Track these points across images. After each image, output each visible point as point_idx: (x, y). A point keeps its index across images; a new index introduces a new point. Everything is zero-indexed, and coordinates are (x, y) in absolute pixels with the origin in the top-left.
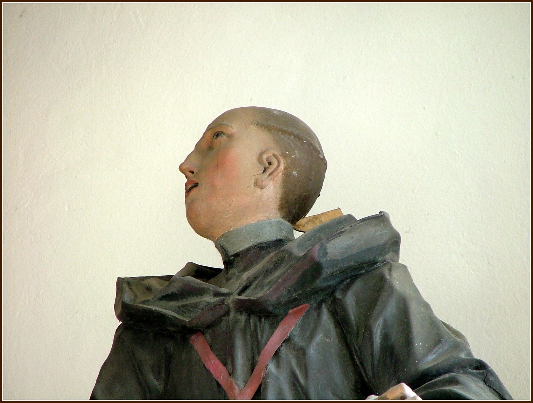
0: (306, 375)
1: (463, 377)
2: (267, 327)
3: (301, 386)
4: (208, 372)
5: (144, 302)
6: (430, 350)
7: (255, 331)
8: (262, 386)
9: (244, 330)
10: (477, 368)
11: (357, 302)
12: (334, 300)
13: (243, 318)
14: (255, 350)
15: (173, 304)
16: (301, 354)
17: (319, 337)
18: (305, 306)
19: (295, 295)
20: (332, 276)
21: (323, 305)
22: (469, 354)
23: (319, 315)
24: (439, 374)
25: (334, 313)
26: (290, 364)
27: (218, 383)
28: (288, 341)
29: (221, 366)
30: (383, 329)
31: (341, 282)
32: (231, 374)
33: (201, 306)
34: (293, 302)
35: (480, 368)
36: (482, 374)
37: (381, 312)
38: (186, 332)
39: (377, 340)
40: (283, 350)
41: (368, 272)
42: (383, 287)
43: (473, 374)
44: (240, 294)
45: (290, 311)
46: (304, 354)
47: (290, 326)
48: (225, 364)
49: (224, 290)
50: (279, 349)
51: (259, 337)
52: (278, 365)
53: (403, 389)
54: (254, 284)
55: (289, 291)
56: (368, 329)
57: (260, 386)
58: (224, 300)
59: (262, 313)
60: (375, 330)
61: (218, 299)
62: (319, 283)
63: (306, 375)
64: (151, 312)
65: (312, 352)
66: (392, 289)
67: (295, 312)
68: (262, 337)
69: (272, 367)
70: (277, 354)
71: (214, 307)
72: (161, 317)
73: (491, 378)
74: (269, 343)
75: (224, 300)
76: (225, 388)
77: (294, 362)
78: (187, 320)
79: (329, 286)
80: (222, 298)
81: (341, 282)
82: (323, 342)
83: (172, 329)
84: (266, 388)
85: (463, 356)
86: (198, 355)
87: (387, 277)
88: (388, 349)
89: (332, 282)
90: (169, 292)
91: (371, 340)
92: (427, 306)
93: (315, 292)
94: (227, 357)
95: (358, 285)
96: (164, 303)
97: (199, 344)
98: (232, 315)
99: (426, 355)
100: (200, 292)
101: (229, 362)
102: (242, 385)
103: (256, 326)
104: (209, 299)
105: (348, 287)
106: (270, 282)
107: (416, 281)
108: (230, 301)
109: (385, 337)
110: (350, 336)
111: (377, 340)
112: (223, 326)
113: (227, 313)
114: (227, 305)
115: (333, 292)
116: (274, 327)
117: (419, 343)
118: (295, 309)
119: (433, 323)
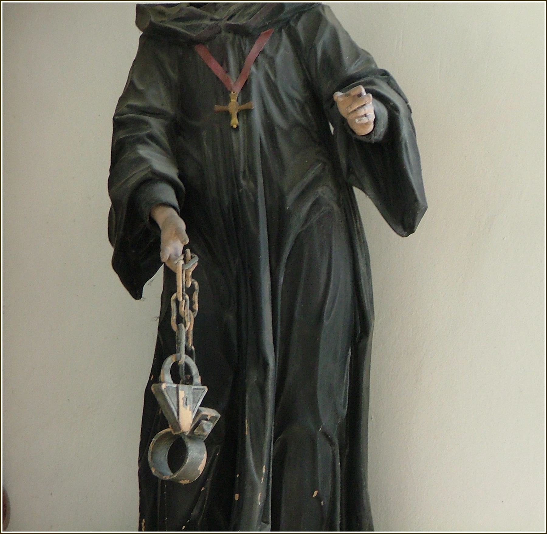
0: (275, 76)
1: (377, 81)
2: (247, 42)
3: (272, 81)
4: (210, 69)
5: (161, 22)
6: (353, 62)
7: (240, 44)
8: (248, 81)
9: (233, 44)
10: (383, 75)
11: (304, 29)
12: (290, 27)
13: (230, 36)
14: (242, 57)
15: (182, 24)
16: (271, 61)
17: (282, 51)
18: (272, 30)
19: (267, 23)
20: (289, 12)
21: (283, 30)
22: (376, 66)
23: (281, 36)
24: (360, 78)
25: (289, 35)
26: (264, 67)
27: (217, 78)
28: (262, 52)
29: (219, 67)
30: (322, 48)
31: (293, 16)
32: (228, 72)
33: (203, 26)
34: (264, 27)
35: (385, 73)
36: (387, 78)
37: (322, 36)
38: (192, 43)
39: (319, 54)
40: (260, 59)
41: (309, 10)
42: (321, 20)
43: (380, 79)
44: (228, 20)
45: (262, 33)
46: (274, 61)
47: (262, 43)
48: (222, 65)
49: (216, 17)
50: (257, 57)
51: (244, 49)
52: (257, 68)
53: (361, 89)
54: (238, 14)
55: (263, 20)
56: (313, 47)
57: (247, 80)
58: (217, 24)
59: (244, 33)
60: (318, 48)
61: (213, 22)
62: (282, 16)
63: (275, 76)
64: (170, 29)
65: (278, 60)
66: (327, 22)
67: (265, 34)
68: (245, 48)
69: (253, 69)
70: (256, 61)
71: (211, 28)
72: (175, 33)
73: (392, 82)
74: (251, 53)
75: (217, 24)
76: (223, 81)
77: (267, 66)
78: (195, 35)
79: (287, 18)
80: (217, 22)
81: (293, 16)
82: (284, 54)
83: (182, 40)
84: (251, 83)
85: (373, 66)
86: (201, 58)
87: (323, 13)
88: (326, 59)
89: (289, 16)
90: (180, 16)
91: (316, 53)
92: (347, 33)
93: (279, 21)
94: (223, 61)
95: (303, 18)
96: (175, 23)
97: (201, 51)
98: (223, 34)
99: (351, 65)
100: (202, 17)
101: (225, 64)
102: (235, 79)
103: (240, 41)
104: (207, 22)
105: (298, 19)
106: (249, 14)
107: (338, 17)
108: (222, 24)
109: (324, 53)
110: (302, 52)
111: (319, 54)
112: (217, 41)
113: (220, 32)
114: (220, 27)
115: (288, 22)
116: (252, 43)
117: (346, 58)
118: (265, 32)
119: (352, 45)
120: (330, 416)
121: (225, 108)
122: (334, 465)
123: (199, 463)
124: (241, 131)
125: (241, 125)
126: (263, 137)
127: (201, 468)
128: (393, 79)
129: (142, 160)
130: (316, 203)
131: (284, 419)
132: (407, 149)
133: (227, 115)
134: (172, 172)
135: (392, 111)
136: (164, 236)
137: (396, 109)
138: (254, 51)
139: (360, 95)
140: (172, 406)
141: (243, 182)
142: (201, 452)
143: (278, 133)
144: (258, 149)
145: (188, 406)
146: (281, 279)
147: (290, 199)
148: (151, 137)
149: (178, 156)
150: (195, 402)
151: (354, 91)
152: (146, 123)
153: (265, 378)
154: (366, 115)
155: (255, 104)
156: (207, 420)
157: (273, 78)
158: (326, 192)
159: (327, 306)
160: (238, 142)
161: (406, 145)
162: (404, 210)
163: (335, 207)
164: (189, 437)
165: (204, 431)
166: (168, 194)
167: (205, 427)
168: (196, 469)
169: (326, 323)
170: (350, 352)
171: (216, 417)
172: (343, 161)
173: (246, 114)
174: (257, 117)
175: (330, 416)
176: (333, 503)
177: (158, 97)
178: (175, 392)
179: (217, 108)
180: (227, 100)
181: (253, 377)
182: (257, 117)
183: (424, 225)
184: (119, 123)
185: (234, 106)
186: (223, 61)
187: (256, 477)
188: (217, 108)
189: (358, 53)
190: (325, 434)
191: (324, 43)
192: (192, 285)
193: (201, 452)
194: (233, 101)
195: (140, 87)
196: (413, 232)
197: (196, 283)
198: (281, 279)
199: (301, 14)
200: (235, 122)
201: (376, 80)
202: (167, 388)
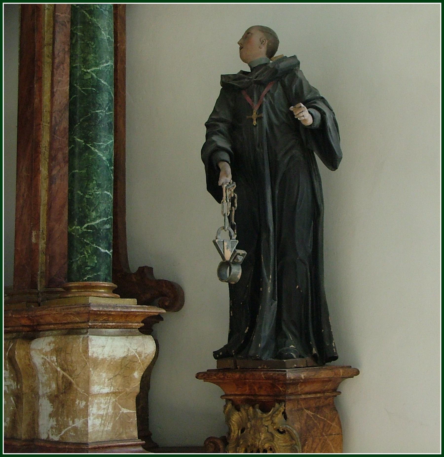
0: (274, 102)
6: (308, 94)
17: (277, 91)
22: (319, 95)
27: (249, 104)
32: (253, 101)
35: (322, 98)
38: (240, 90)
39: (294, 91)
40: (268, 95)
52: (266, 99)
69: (264, 99)
72: (233, 86)
77: (270, 98)
88: (296, 93)
92: (307, 82)
94: (252, 97)
97: (244, 93)
109: (296, 90)
111: (294, 91)
117: (305, 92)
119: (309, 86)
120: (303, 252)
121: (250, 117)
122: (307, 273)
123: (238, 275)
124: (257, 127)
125: (258, 124)
126: (268, 129)
127: (239, 277)
128: (326, 101)
129: (214, 141)
130: (292, 157)
131: (281, 253)
132: (330, 131)
133: (252, 120)
134: (227, 146)
135: (323, 114)
136: (221, 173)
137: (325, 113)
138: (265, 92)
139: (301, 107)
140: (221, 249)
141: (258, 149)
142: (239, 270)
143: (275, 127)
144: (265, 134)
145: (229, 250)
146: (277, 192)
147: (280, 156)
148: (220, 132)
149: (232, 139)
150: (232, 247)
151: (297, 106)
152: (218, 125)
153: (269, 236)
154: (303, 116)
155: (264, 115)
156: (240, 255)
157: (273, 103)
158: (297, 152)
159: (298, 203)
160: (256, 131)
161: (330, 129)
162: (333, 161)
163: (302, 159)
164: (232, 263)
165: (238, 260)
166: (226, 157)
167: (239, 258)
168: (236, 277)
169: (298, 211)
170: (313, 223)
171: (244, 254)
172: (304, 138)
173: (260, 119)
174: (265, 120)
175: (303, 252)
176: (307, 291)
177: (225, 115)
178: (222, 243)
179: (247, 117)
180: (252, 114)
181: (264, 236)
182: (265, 120)
183: (342, 165)
184: (207, 125)
185: (254, 115)
186: (252, 97)
187: (267, 280)
188: (247, 117)
189: (311, 90)
190: (301, 260)
191: (296, 86)
192: (234, 196)
193: (239, 270)
194: (255, 114)
195: (218, 110)
196: (337, 168)
197: (236, 195)
198: (277, 192)
199: (287, 74)
200: (255, 123)
201: (313, 101)
202: (219, 241)
